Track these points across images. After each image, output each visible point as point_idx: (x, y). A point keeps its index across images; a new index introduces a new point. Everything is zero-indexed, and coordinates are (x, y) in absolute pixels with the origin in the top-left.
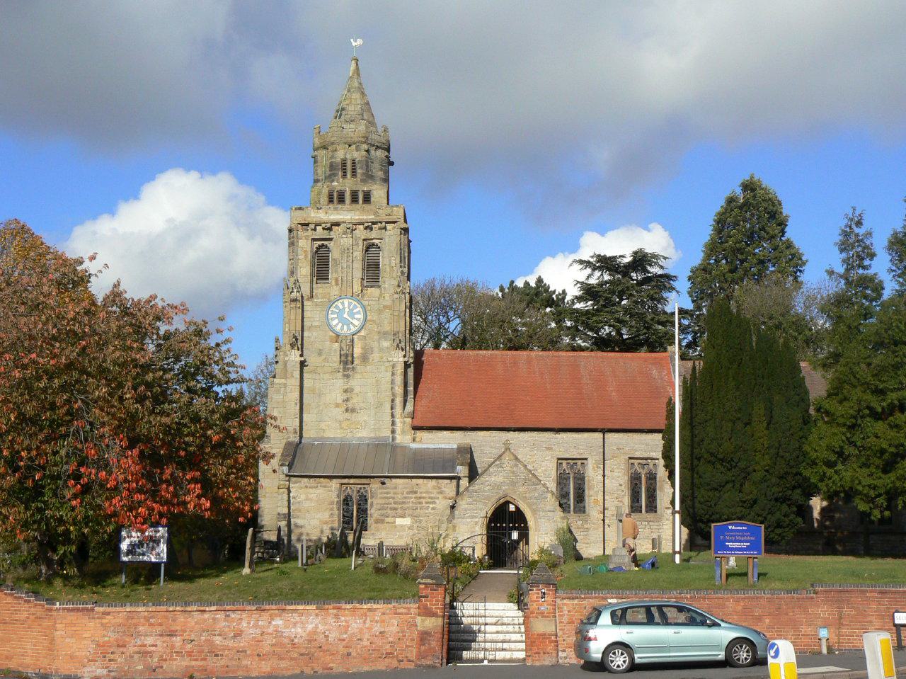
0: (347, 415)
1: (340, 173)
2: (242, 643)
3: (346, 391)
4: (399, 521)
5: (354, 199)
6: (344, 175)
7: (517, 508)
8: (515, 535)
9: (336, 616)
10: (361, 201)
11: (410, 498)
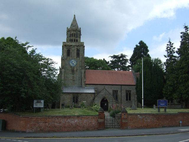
0: (73, 82)
2: (61, 125)
6: (73, 36)
7: (106, 99)
8: (106, 104)
9: (81, 119)
10: (73, 41)
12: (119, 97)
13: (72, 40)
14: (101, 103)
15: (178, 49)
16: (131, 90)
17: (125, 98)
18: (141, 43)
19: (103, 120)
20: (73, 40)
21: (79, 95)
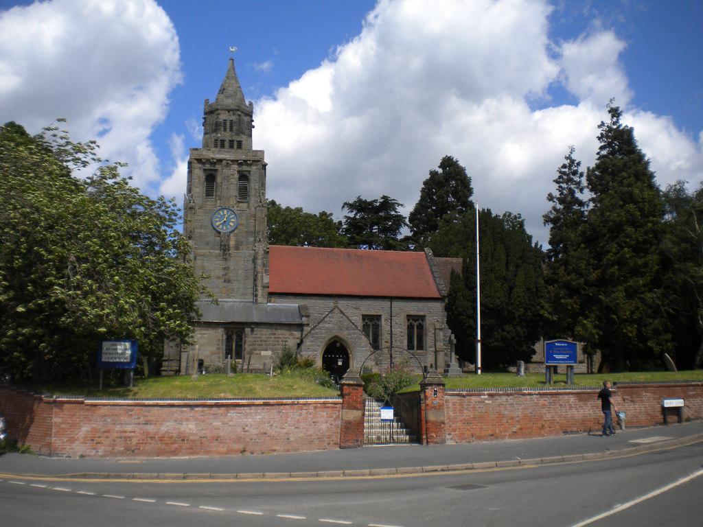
1: (222, 129)
3: (225, 269)
4: (263, 353)
5: (231, 146)
6: (225, 130)
7: (341, 344)
10: (235, 147)
11: (271, 338)
12: (385, 336)
13: (223, 141)
14: (324, 357)
15: (588, 168)
16: (422, 313)
17: (406, 342)
18: (448, 163)
19: (359, 413)
20: (227, 144)
21: (248, 330)
